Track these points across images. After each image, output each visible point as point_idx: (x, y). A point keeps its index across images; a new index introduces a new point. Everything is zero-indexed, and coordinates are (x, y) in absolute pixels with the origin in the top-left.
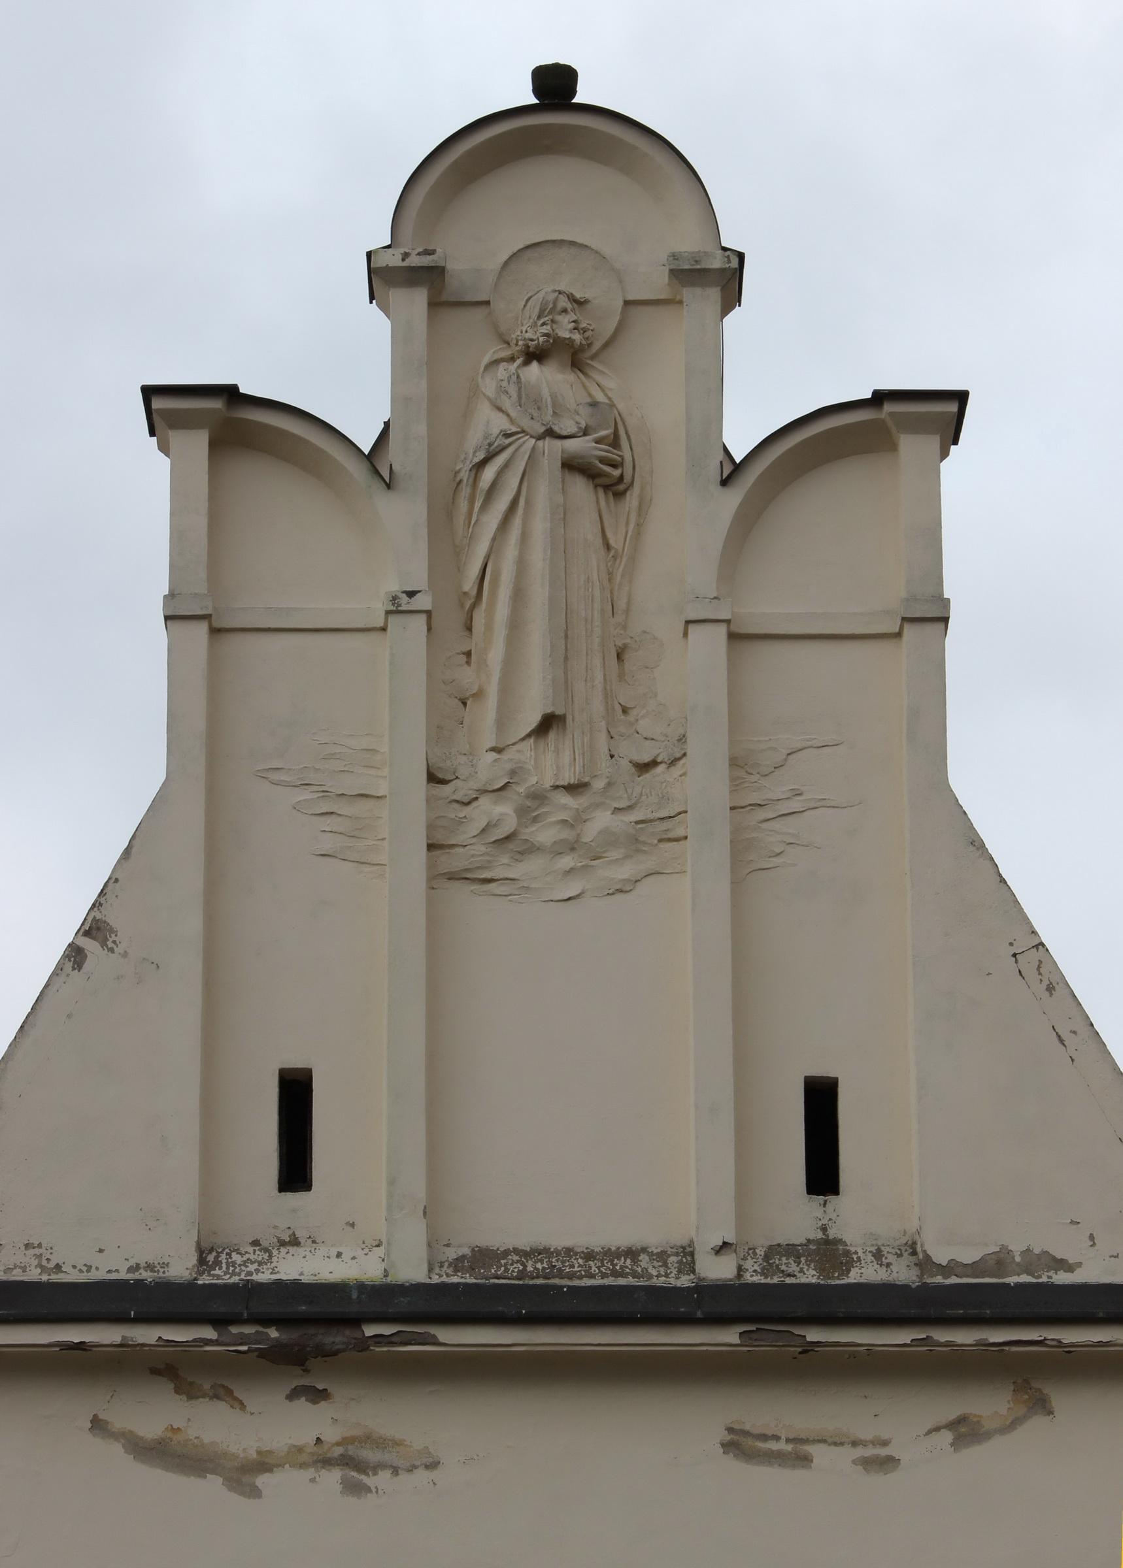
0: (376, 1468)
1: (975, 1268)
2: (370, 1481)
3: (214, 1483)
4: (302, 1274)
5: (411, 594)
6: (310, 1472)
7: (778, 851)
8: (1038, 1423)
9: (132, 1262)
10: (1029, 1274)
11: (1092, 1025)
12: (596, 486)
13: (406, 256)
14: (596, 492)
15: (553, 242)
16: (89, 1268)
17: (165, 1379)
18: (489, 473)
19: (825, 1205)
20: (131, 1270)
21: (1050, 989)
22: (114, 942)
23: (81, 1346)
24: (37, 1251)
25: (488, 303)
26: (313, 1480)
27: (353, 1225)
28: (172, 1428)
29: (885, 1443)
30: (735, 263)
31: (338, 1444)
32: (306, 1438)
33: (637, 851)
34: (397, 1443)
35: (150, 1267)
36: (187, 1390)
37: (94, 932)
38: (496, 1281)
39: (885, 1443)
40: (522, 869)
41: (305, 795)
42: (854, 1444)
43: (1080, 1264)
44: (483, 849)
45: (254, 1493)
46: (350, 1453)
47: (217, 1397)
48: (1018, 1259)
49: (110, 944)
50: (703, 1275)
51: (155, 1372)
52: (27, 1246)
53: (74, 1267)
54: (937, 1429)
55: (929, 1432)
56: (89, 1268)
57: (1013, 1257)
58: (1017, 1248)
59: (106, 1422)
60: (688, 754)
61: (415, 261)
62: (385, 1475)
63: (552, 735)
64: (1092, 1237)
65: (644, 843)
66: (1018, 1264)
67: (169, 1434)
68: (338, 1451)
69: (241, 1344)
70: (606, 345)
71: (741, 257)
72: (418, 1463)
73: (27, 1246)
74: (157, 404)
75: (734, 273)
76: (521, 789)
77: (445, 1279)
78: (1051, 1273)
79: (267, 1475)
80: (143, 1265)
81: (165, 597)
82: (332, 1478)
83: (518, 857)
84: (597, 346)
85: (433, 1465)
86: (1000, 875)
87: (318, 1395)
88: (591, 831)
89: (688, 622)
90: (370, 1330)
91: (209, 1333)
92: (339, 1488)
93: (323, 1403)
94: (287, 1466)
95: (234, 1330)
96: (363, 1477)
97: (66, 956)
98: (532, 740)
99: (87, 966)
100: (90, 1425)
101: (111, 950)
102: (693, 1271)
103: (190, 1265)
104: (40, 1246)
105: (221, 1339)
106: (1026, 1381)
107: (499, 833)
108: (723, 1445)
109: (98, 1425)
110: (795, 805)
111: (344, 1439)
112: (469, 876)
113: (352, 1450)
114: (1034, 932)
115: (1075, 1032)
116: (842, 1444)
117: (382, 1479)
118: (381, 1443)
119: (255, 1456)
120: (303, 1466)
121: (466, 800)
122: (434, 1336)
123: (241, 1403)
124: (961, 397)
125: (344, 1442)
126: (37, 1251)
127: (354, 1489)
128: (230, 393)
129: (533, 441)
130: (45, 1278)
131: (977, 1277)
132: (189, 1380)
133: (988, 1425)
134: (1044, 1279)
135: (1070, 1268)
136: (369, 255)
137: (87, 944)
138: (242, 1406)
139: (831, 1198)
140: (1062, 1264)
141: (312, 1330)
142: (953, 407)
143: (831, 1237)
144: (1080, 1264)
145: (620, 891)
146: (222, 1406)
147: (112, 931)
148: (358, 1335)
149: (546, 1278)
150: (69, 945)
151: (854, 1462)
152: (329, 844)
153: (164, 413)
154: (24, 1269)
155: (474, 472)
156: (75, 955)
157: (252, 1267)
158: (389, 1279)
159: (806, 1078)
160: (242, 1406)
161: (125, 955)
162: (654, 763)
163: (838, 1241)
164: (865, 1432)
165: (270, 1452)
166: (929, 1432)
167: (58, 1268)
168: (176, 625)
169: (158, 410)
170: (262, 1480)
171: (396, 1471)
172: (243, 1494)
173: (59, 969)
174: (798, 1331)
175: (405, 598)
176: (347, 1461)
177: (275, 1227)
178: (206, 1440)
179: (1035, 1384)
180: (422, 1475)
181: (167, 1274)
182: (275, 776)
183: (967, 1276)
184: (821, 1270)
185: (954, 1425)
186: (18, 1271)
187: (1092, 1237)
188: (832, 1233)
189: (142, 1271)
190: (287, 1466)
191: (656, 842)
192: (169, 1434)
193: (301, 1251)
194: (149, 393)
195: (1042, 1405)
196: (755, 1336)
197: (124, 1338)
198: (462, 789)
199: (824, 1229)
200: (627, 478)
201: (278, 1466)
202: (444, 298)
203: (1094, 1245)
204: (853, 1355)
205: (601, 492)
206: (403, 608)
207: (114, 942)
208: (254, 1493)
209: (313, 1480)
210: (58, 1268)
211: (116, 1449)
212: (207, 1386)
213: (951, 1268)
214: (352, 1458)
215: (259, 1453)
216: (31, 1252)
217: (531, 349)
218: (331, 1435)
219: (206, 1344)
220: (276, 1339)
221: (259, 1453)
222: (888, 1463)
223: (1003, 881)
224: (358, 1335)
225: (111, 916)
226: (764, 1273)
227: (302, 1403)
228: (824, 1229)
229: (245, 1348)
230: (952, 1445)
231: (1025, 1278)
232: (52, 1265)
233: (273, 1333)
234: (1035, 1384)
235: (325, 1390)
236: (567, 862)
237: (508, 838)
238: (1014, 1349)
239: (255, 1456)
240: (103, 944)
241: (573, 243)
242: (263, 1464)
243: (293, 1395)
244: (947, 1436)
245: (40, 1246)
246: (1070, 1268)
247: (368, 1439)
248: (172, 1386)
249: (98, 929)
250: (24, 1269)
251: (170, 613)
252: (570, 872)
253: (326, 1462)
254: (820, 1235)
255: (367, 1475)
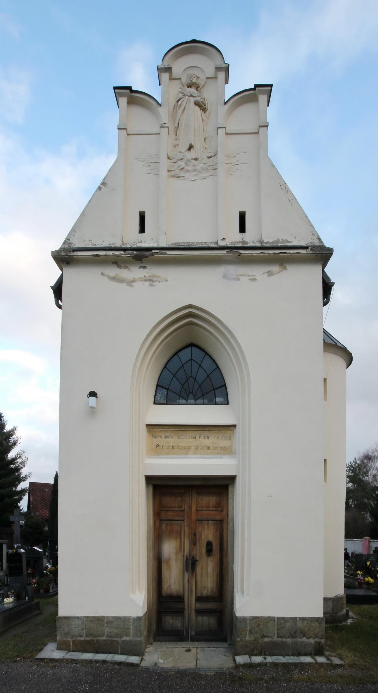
0: (155, 282)
1: (272, 243)
2: (154, 284)
3: (124, 284)
4: (151, 280)
5: (165, 124)
6: (143, 282)
7: (235, 171)
8: (284, 271)
9: (109, 243)
10: (283, 244)
11: (295, 198)
12: (201, 109)
13: (164, 66)
14: (201, 110)
15: (193, 67)
16: (101, 244)
17: (115, 265)
18: (180, 102)
19: (243, 234)
20: (109, 245)
21: (287, 191)
22: (107, 186)
23: (97, 255)
24: (91, 242)
25: (180, 79)
26: (144, 284)
27: (153, 239)
28: (117, 274)
29: (254, 276)
30: (227, 66)
31: (148, 277)
32: (142, 276)
33: (208, 171)
34: (160, 277)
35: (113, 244)
36: (119, 266)
37: (103, 184)
38: (179, 246)
39: (254, 276)
40: (186, 175)
41: (145, 163)
42: (248, 276)
43: (293, 242)
44: (178, 170)
45: (132, 286)
46: (151, 279)
47: (125, 268)
48: (281, 241)
49: (106, 186)
50: (219, 244)
51: (113, 263)
52: (89, 241)
53: (98, 244)
54: (264, 273)
55: (263, 274)
56: (101, 244)
57: (280, 241)
58: (280, 239)
59: (104, 273)
60: (218, 168)
61: (166, 66)
62: (157, 283)
63: (192, 150)
64: (295, 237)
65: (209, 170)
66: (281, 242)
67: (116, 275)
68: (148, 278)
69: (128, 255)
70: (203, 87)
71: (229, 65)
72: (164, 280)
73: (89, 241)
74: (116, 91)
75: (227, 68)
76: (185, 159)
77: (169, 246)
78: (287, 243)
79: (135, 283)
80: (111, 244)
81: (118, 125)
82: (147, 283)
83: (185, 173)
84: (201, 87)
85: (166, 281)
86: (278, 172)
87: (145, 267)
88: (198, 168)
89: (218, 128)
90: (154, 251)
91: (122, 252)
92: (148, 285)
93: (146, 269)
94: (138, 281)
95: (127, 252)
96: (153, 283)
97: (98, 188)
98: (188, 151)
99: (102, 190)
100: (101, 274)
101: (106, 187)
102: (218, 244)
103: (120, 244)
104: (92, 241)
105: (125, 254)
106: (282, 264)
107: (181, 168)
108: (223, 276)
109: (102, 274)
110: (237, 163)
111: (149, 276)
112: (176, 176)
113: (151, 278)
114: (284, 181)
115: (292, 199)
116: (246, 276)
117: (156, 284)
118: (157, 277)
119: (132, 279)
120: (141, 281)
121: (175, 162)
122: (166, 253)
123: (130, 269)
124: (271, 86)
125: (150, 276)
126: (91, 242)
127: (152, 285)
128: (129, 88)
129: (188, 97)
130: (93, 246)
131: (273, 244)
132: (120, 265)
133: (274, 272)
134: (286, 245)
135: (291, 243)
136: (157, 66)
137: (102, 186)
138: (130, 270)
139: (244, 234)
140: (289, 242)
141: (142, 252)
142: (270, 88)
143: (244, 240)
144: (293, 242)
145: (204, 179)
146: (126, 270)
147: (107, 184)
148: (151, 252)
149: (189, 245)
150: (99, 187)
151: (248, 279)
152: (149, 171)
153: (118, 93)
154: (89, 245)
155: (177, 103)
156: (100, 188)
157: (132, 245)
158: (159, 246)
159: (240, 212)
160: (130, 270)
161: (109, 188)
162: (210, 153)
163: (245, 241)
164: (251, 274)
165: (135, 279)
166: (263, 274)
167: (95, 245)
168: (120, 131)
169: (116, 92)
170: (134, 284)
171: (159, 282)
172: (130, 286)
173: (96, 191)
174: (238, 251)
175: (163, 124)
176: (150, 280)
177: (138, 240)
178: (123, 276)
179: (284, 264)
180: (164, 283)
181: (116, 245)
182: (138, 159)
183: (271, 244)
184: (242, 244)
185: (268, 272)
186: (88, 245)
187: (295, 237)
188: (244, 240)
189: (111, 245)
190: (138, 281)
191: (211, 169)
192: (116, 275)
193: (142, 243)
194: (115, 88)
195: (285, 268)
196: (229, 252)
197: (106, 254)
198: (174, 160)
199: (243, 239)
200: (207, 108)
201: (137, 281)
202: (172, 77)
203: (295, 238)
204: (248, 257)
205: (202, 111)
206: (163, 126)
207: (107, 186)
208: (132, 286)
209: (144, 284)
210: (95, 245)
211: (106, 278)
212: (123, 266)
213: (266, 243)
214: (151, 280)
215: (133, 279)
216: (91, 242)
217: (189, 85)
218: (147, 275)
219: (122, 255)
220: (135, 254)
221: (133, 279)
222: (255, 280)
223: (278, 172)
224: (151, 252)
225: (107, 181)
226: (231, 245)
227: (142, 269)
228: (243, 239)
229: (129, 255)
230: (267, 276)
231: (282, 244)
232: (94, 244)
233: (135, 252)
234: (284, 264)
235: (146, 267)
236: (195, 173)
237: (183, 168)
238: (281, 254)
239: (132, 279)
240: (105, 186)
241: (197, 67)
242: (134, 281)
243: (141, 267)
244: (266, 274)
245: (92, 241)
246: (291, 243)
247: (154, 276)
248: (117, 266)
249: (104, 184)
250: (89, 245)
251: (119, 128)
252: (195, 175)
253: (146, 280)
254: (242, 240)
255: (154, 283)
